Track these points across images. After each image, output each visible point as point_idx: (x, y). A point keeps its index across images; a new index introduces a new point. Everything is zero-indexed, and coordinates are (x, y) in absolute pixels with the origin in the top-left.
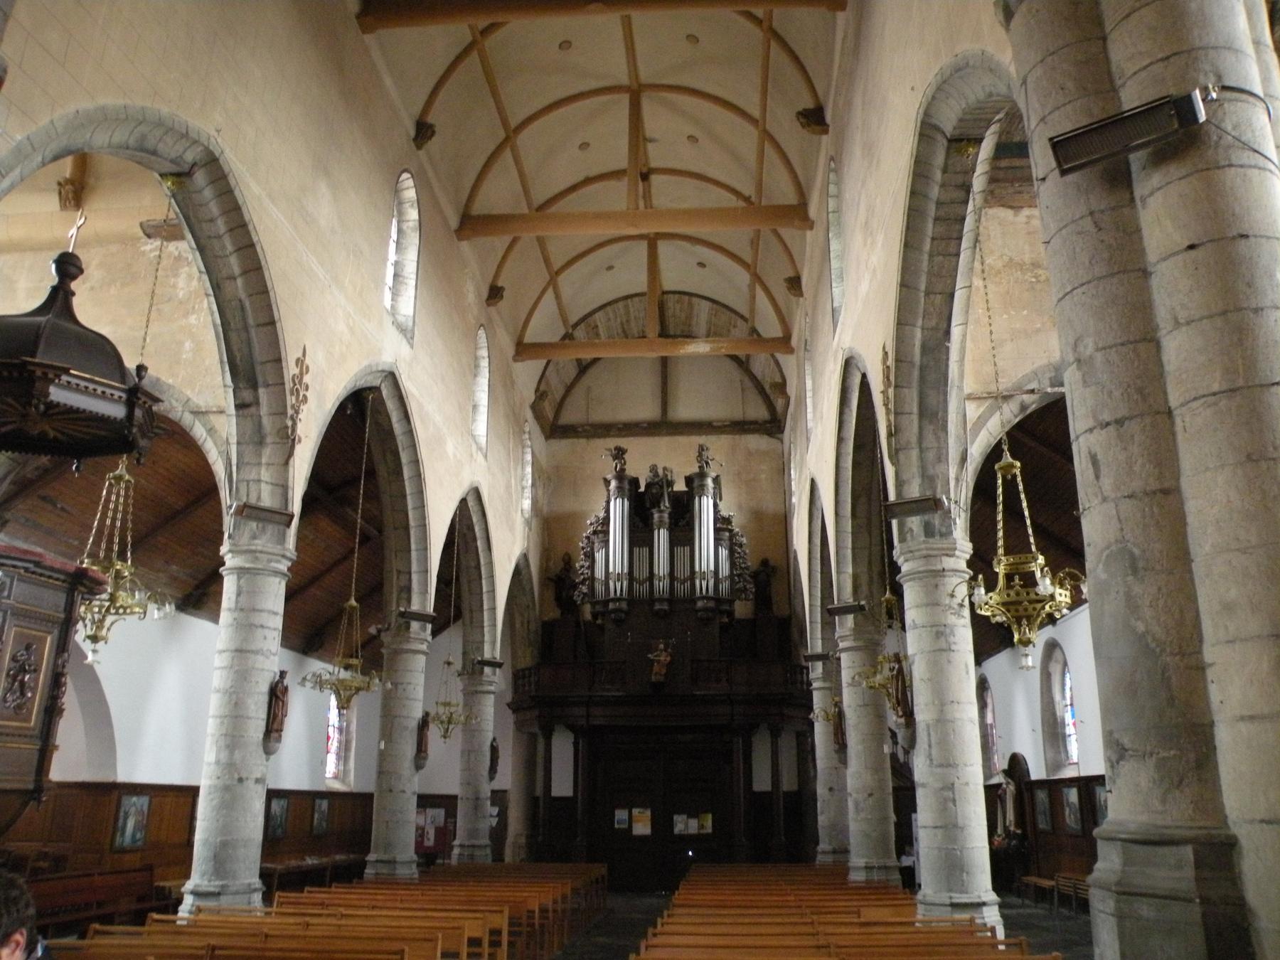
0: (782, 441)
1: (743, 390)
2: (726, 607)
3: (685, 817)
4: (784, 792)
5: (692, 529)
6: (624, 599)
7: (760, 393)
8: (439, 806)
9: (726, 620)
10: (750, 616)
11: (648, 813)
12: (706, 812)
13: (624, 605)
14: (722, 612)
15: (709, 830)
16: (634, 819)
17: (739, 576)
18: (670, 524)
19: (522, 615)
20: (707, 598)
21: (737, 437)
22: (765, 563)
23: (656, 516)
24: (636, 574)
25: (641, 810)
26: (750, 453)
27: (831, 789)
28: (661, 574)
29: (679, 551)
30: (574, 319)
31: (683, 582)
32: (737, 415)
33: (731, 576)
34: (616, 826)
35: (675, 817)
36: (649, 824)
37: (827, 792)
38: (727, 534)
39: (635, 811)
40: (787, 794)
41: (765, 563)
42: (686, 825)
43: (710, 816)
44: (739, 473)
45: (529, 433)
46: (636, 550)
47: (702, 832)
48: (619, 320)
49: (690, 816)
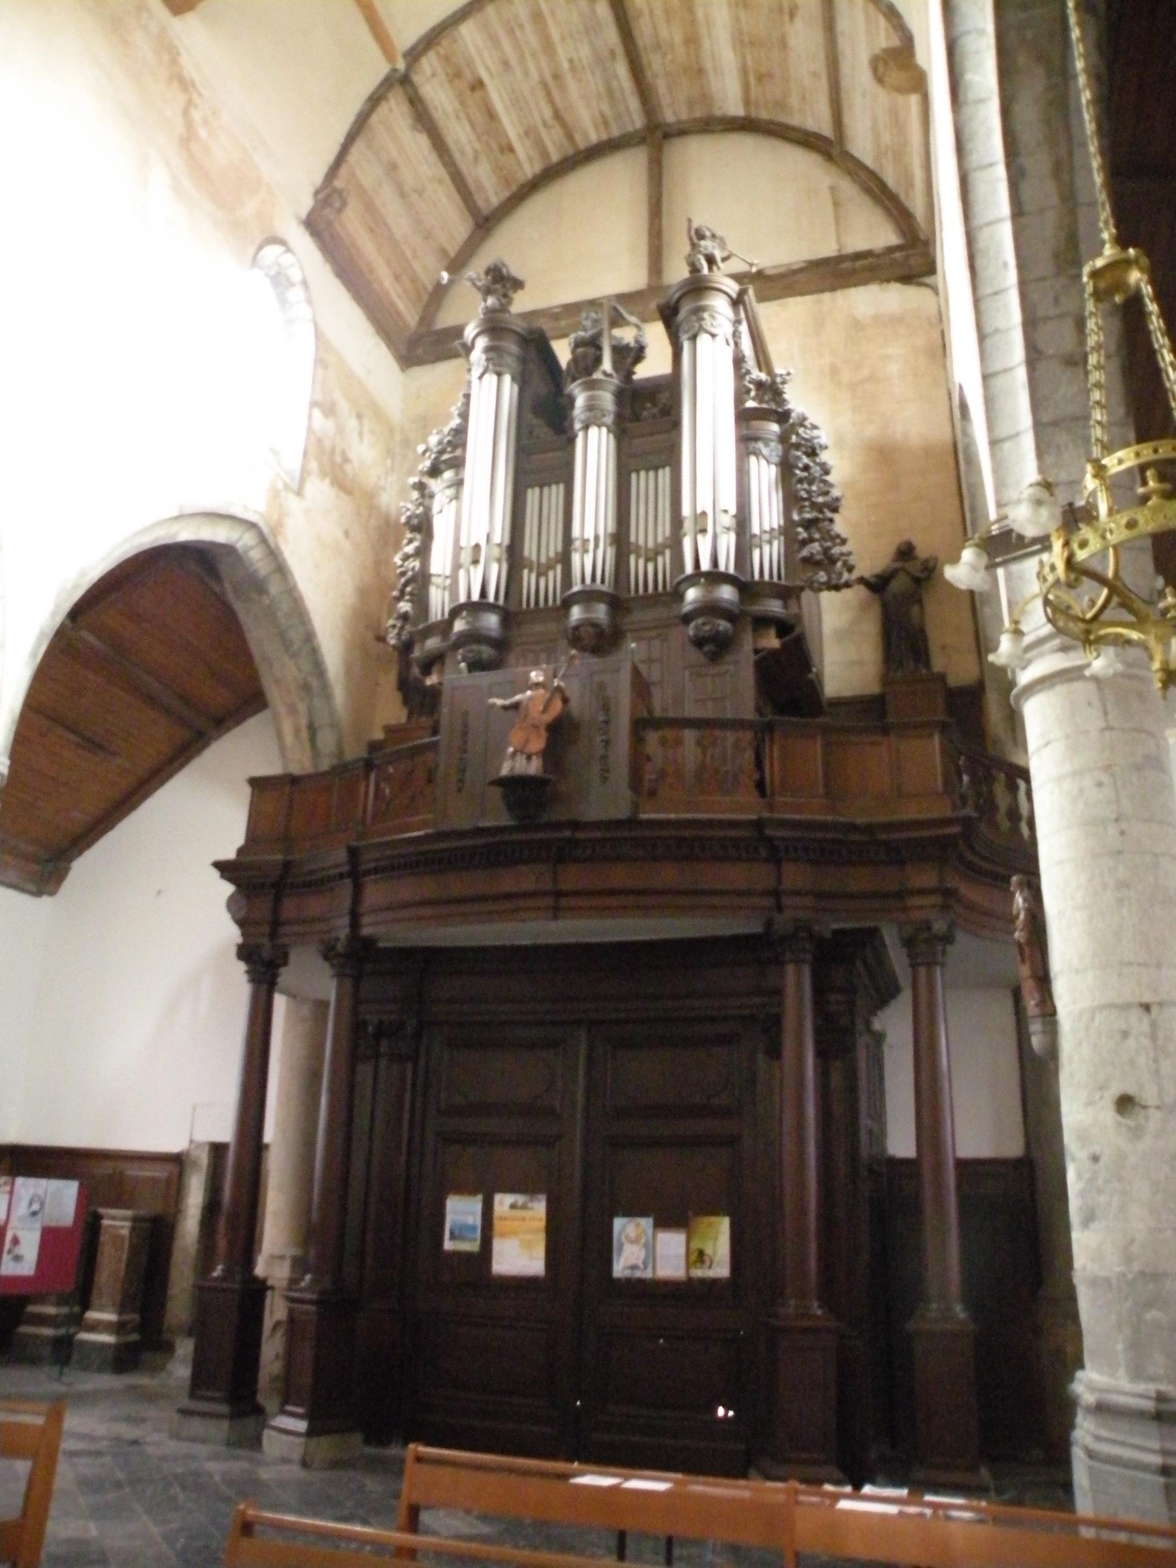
0: (935, 289)
1: (836, 204)
2: (774, 607)
3: (646, 1223)
4: (965, 1167)
5: (677, 424)
6: (493, 608)
7: (868, 191)
8: (65, 1174)
9: (772, 641)
10: (873, 687)
11: (539, 1208)
12: (713, 1210)
13: (492, 621)
14: (762, 622)
15: (721, 1269)
16: (497, 1224)
17: (809, 524)
18: (619, 417)
19: (292, 709)
20: (715, 577)
21: (826, 297)
22: (906, 552)
23: (580, 401)
24: (529, 549)
25: (519, 1199)
26: (857, 325)
27: (1125, 1103)
28: (589, 534)
29: (641, 481)
30: (407, 35)
31: (652, 556)
32: (827, 249)
33: (787, 530)
34: (448, 1245)
35: (618, 1223)
36: (540, 1251)
37: (1108, 1115)
38: (775, 427)
39: (503, 1202)
40: (968, 1168)
41: (906, 552)
42: (651, 1250)
43: (724, 1225)
44: (834, 371)
45: (305, 283)
46: (532, 495)
47: (698, 1273)
48: (535, 76)
49: (663, 1223)
